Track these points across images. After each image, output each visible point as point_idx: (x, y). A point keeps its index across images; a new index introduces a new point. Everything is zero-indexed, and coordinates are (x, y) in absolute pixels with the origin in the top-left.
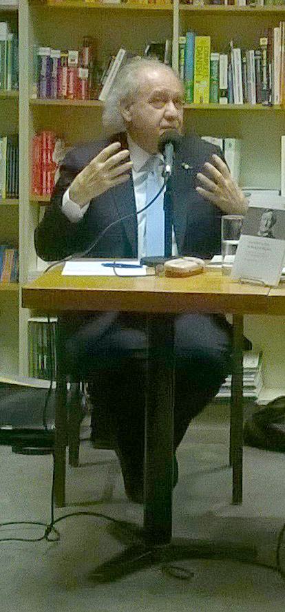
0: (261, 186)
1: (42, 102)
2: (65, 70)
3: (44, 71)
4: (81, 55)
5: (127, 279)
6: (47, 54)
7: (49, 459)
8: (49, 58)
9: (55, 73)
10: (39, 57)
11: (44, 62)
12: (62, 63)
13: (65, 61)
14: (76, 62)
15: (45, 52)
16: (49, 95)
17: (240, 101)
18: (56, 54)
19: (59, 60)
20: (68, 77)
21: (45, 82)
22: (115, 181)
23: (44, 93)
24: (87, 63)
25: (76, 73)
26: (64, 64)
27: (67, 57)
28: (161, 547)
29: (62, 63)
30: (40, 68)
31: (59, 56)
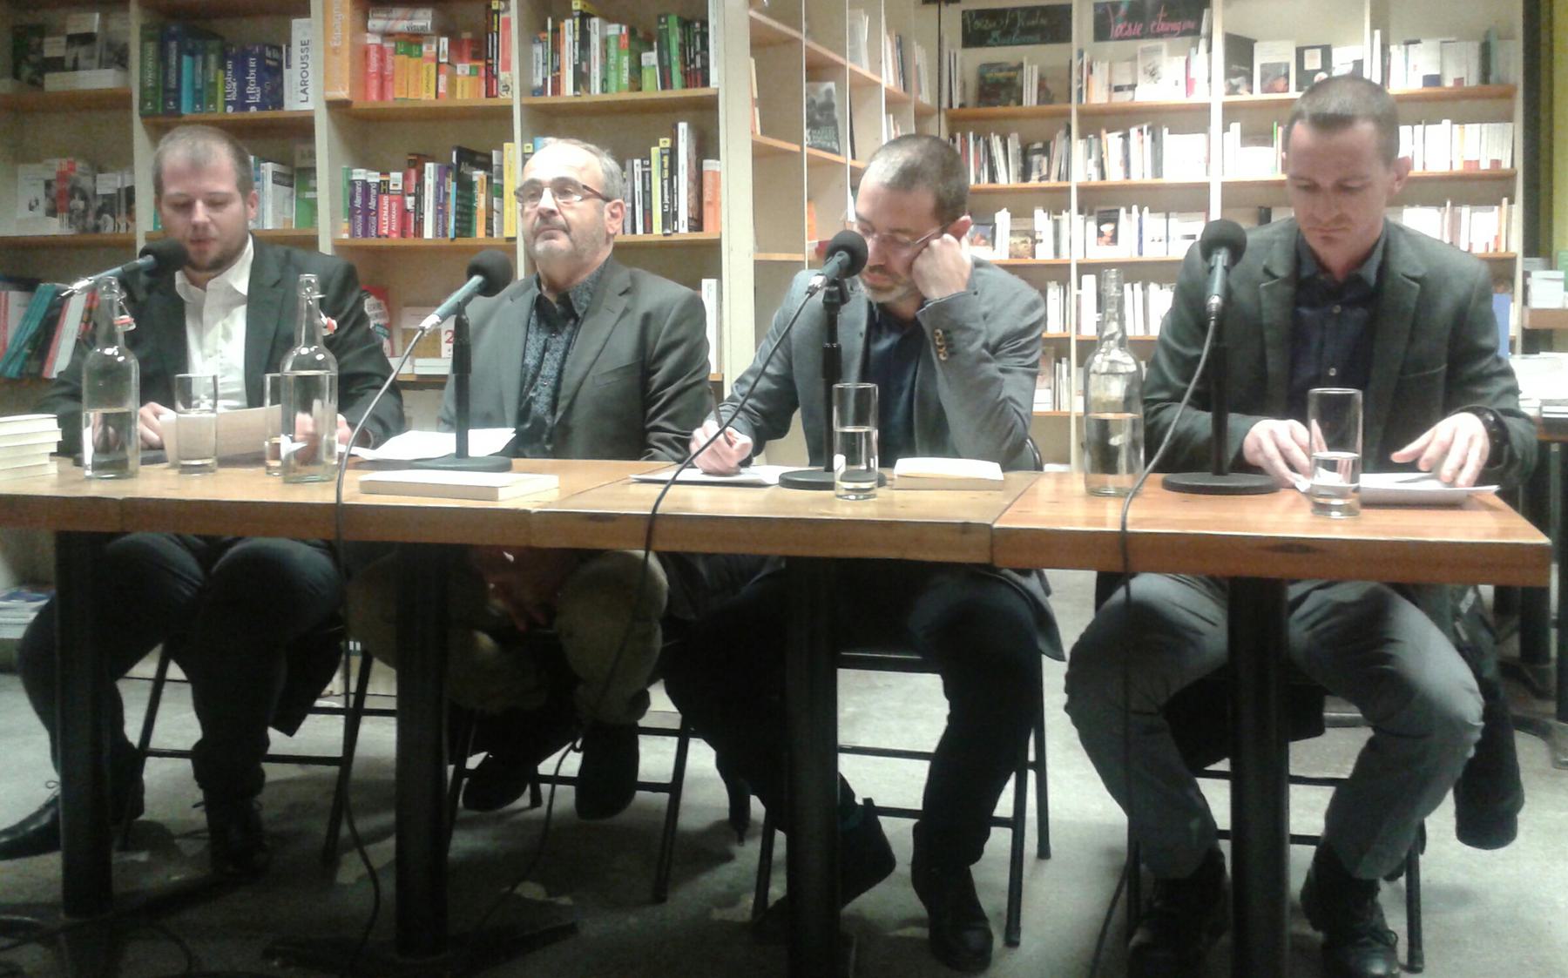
0: (785, 325)
1: (361, 241)
2: (386, 199)
3: (358, 202)
4: (406, 178)
5: (915, 480)
6: (363, 178)
7: (919, 807)
8: (366, 185)
9: (372, 204)
10: (352, 183)
11: (359, 189)
12: (383, 188)
13: (386, 187)
14: (400, 187)
15: (360, 174)
16: (366, 233)
17: (634, 231)
18: (374, 177)
19: (379, 184)
20: (390, 208)
21: (360, 217)
22: (1402, 277)
23: (359, 231)
24: (413, 191)
25: (403, 203)
26: (384, 190)
27: (388, 181)
28: (164, 539)
29: (383, 188)
30: (352, 198)
31: (377, 180)
